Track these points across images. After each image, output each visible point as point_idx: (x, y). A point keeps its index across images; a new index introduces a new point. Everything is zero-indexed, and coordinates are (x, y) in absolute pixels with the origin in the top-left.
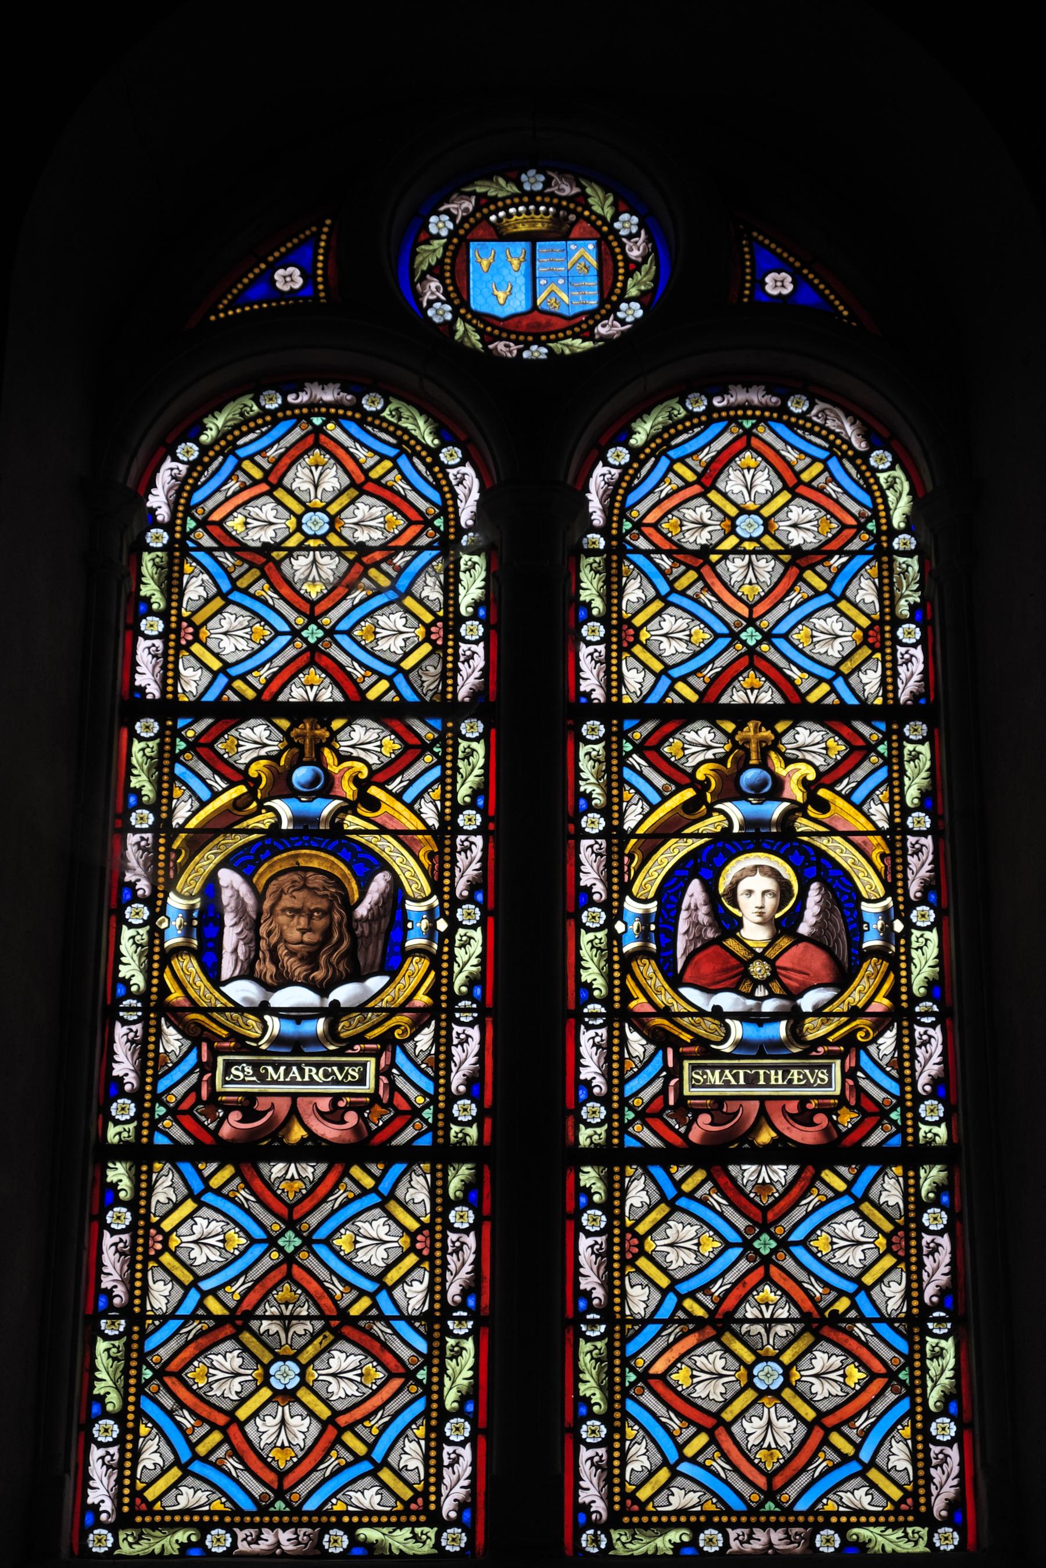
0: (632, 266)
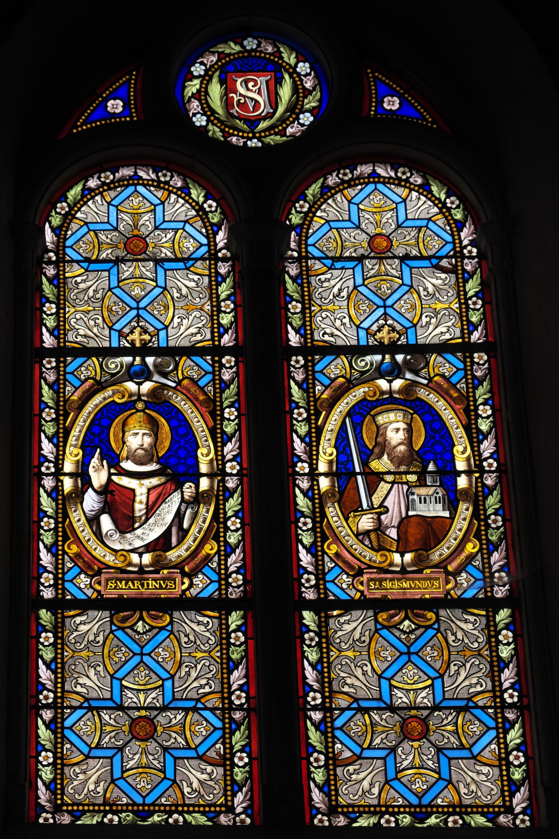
0: (306, 92)
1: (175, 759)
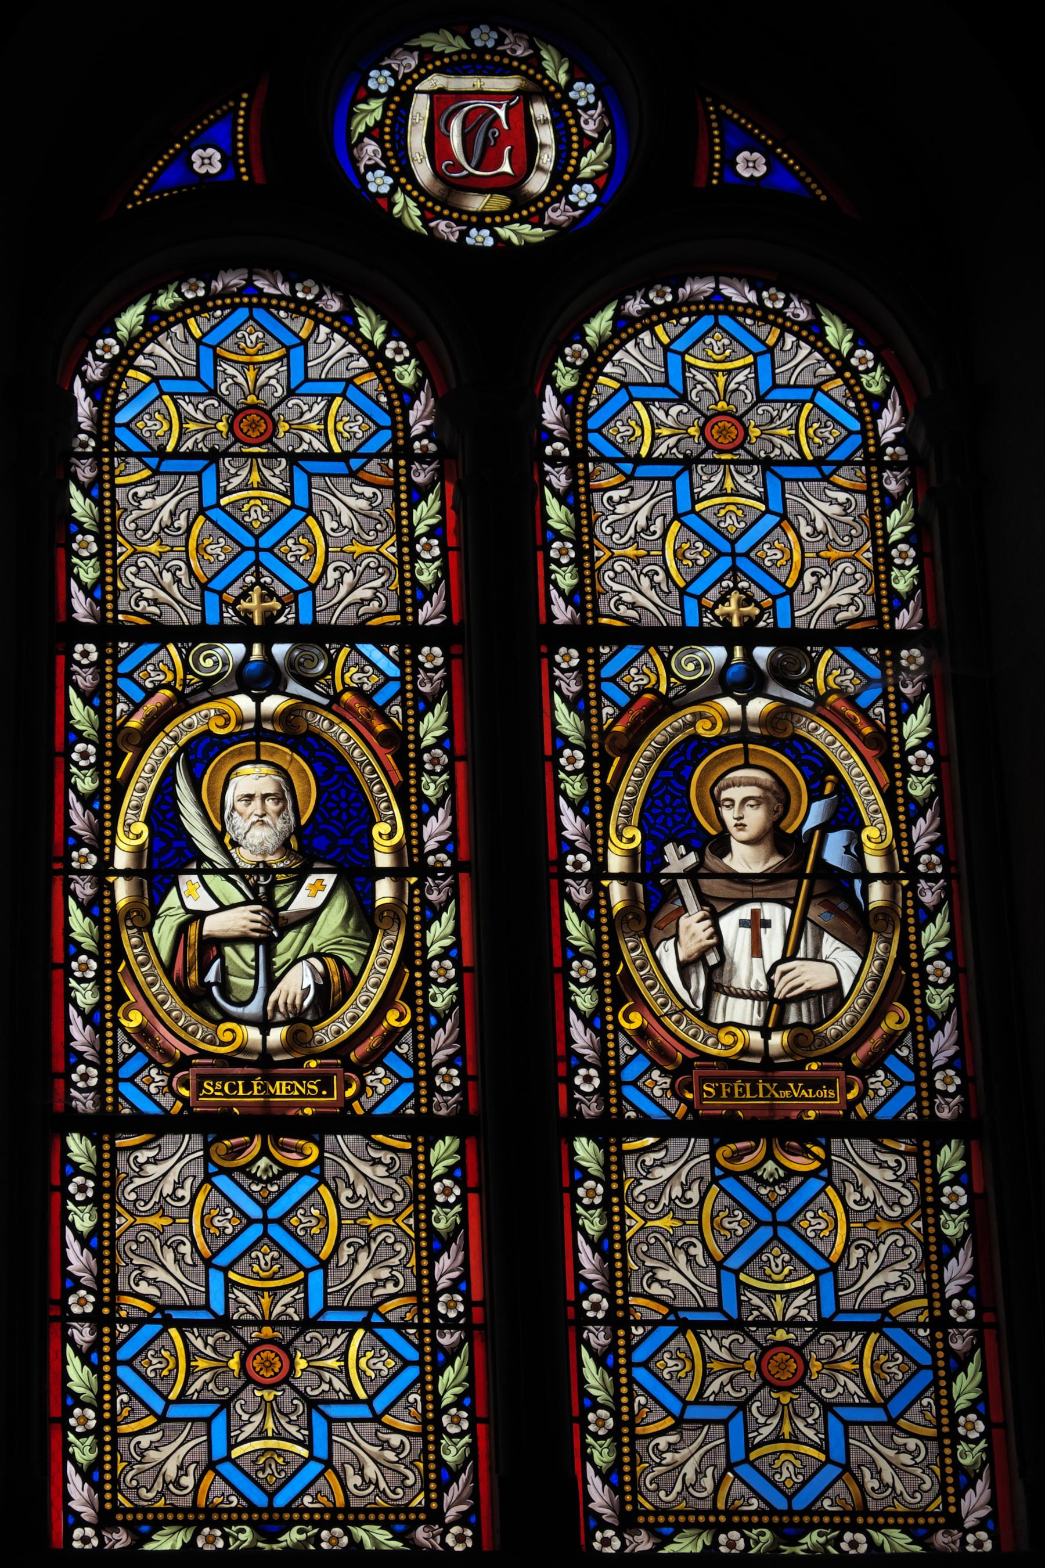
1: (847, 1424)
